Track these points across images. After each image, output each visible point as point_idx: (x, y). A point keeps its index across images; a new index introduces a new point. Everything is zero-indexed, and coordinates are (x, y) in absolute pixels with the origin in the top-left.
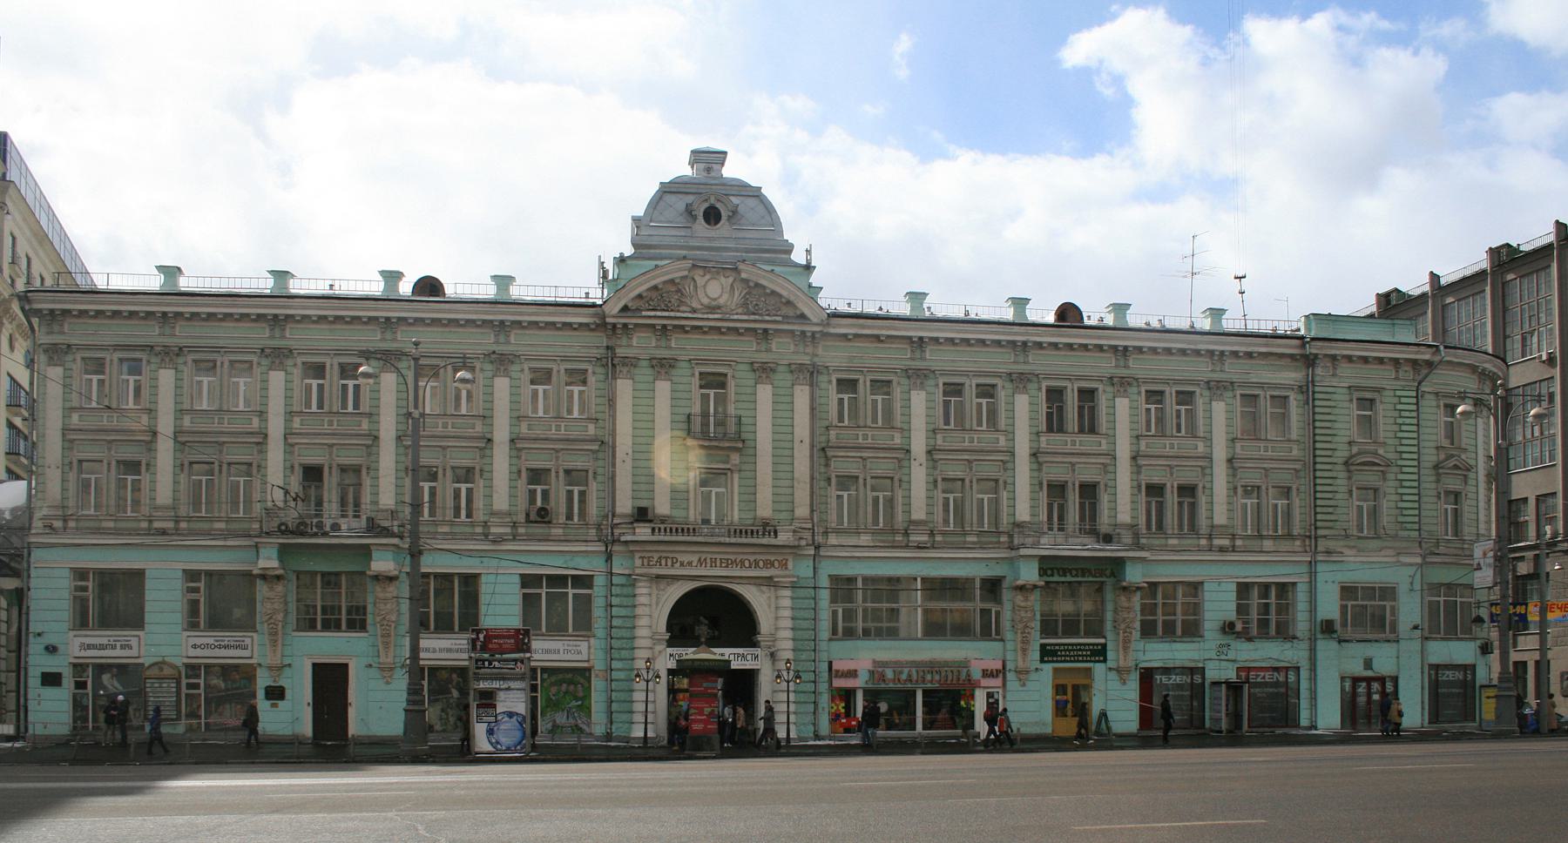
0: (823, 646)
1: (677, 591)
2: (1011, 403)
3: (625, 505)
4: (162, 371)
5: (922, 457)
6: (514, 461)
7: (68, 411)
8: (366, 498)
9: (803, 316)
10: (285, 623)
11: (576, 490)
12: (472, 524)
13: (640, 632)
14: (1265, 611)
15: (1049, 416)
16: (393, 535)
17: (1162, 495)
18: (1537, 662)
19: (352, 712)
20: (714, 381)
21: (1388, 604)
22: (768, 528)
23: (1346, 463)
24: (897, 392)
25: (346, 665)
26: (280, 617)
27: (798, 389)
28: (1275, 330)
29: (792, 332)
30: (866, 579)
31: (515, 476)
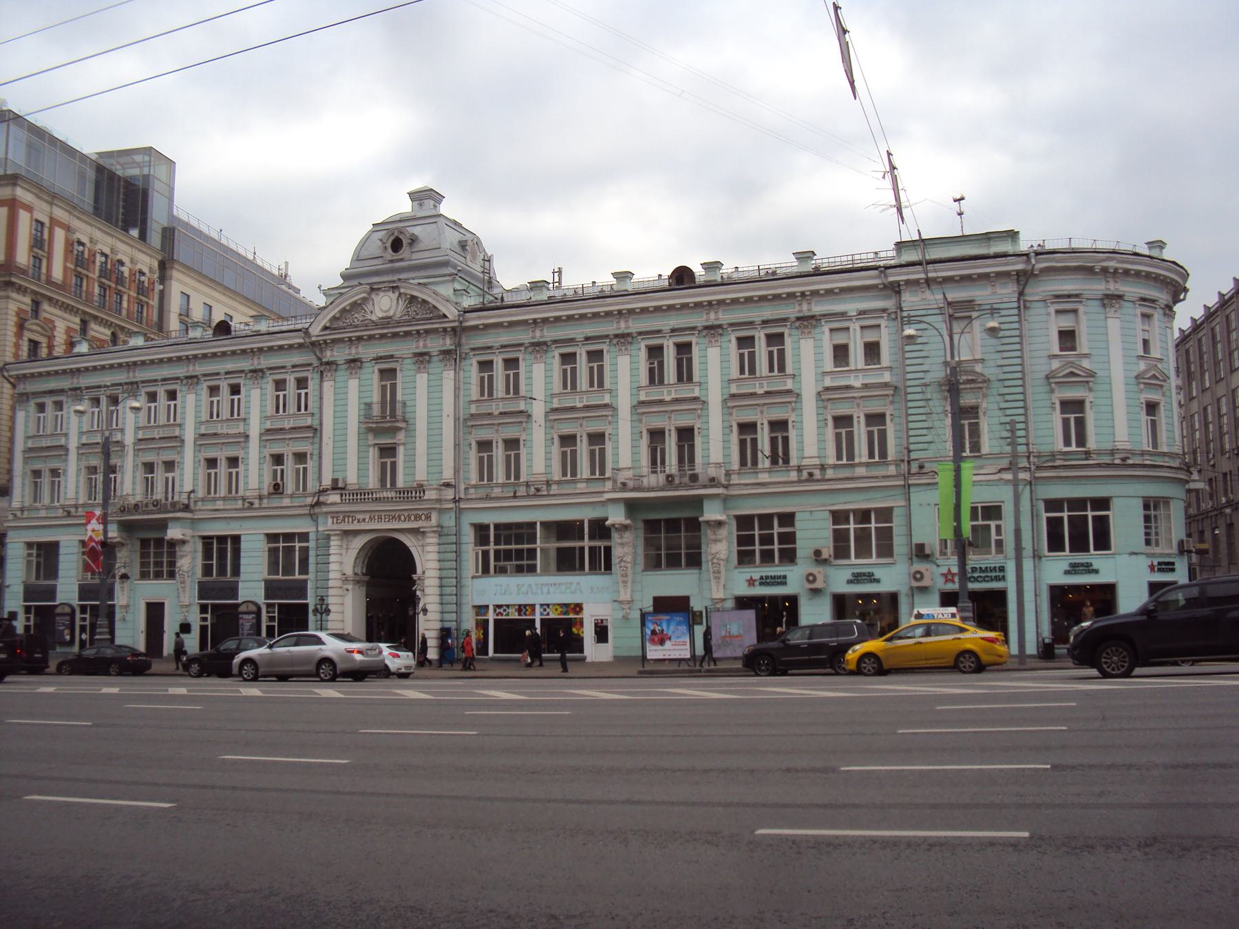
0: (467, 582)
1: (359, 542)
5: (541, 421)
7: (81, 433)
9: (445, 316)
10: (634, 563)
12: (886, 464)
13: (332, 575)
15: (651, 371)
18: (1174, 583)
20: (388, 374)
21: (993, 524)
22: (421, 488)
23: (1047, 377)
25: (163, 604)
26: (629, 559)
27: (445, 374)
30: (497, 526)
31: (549, 443)
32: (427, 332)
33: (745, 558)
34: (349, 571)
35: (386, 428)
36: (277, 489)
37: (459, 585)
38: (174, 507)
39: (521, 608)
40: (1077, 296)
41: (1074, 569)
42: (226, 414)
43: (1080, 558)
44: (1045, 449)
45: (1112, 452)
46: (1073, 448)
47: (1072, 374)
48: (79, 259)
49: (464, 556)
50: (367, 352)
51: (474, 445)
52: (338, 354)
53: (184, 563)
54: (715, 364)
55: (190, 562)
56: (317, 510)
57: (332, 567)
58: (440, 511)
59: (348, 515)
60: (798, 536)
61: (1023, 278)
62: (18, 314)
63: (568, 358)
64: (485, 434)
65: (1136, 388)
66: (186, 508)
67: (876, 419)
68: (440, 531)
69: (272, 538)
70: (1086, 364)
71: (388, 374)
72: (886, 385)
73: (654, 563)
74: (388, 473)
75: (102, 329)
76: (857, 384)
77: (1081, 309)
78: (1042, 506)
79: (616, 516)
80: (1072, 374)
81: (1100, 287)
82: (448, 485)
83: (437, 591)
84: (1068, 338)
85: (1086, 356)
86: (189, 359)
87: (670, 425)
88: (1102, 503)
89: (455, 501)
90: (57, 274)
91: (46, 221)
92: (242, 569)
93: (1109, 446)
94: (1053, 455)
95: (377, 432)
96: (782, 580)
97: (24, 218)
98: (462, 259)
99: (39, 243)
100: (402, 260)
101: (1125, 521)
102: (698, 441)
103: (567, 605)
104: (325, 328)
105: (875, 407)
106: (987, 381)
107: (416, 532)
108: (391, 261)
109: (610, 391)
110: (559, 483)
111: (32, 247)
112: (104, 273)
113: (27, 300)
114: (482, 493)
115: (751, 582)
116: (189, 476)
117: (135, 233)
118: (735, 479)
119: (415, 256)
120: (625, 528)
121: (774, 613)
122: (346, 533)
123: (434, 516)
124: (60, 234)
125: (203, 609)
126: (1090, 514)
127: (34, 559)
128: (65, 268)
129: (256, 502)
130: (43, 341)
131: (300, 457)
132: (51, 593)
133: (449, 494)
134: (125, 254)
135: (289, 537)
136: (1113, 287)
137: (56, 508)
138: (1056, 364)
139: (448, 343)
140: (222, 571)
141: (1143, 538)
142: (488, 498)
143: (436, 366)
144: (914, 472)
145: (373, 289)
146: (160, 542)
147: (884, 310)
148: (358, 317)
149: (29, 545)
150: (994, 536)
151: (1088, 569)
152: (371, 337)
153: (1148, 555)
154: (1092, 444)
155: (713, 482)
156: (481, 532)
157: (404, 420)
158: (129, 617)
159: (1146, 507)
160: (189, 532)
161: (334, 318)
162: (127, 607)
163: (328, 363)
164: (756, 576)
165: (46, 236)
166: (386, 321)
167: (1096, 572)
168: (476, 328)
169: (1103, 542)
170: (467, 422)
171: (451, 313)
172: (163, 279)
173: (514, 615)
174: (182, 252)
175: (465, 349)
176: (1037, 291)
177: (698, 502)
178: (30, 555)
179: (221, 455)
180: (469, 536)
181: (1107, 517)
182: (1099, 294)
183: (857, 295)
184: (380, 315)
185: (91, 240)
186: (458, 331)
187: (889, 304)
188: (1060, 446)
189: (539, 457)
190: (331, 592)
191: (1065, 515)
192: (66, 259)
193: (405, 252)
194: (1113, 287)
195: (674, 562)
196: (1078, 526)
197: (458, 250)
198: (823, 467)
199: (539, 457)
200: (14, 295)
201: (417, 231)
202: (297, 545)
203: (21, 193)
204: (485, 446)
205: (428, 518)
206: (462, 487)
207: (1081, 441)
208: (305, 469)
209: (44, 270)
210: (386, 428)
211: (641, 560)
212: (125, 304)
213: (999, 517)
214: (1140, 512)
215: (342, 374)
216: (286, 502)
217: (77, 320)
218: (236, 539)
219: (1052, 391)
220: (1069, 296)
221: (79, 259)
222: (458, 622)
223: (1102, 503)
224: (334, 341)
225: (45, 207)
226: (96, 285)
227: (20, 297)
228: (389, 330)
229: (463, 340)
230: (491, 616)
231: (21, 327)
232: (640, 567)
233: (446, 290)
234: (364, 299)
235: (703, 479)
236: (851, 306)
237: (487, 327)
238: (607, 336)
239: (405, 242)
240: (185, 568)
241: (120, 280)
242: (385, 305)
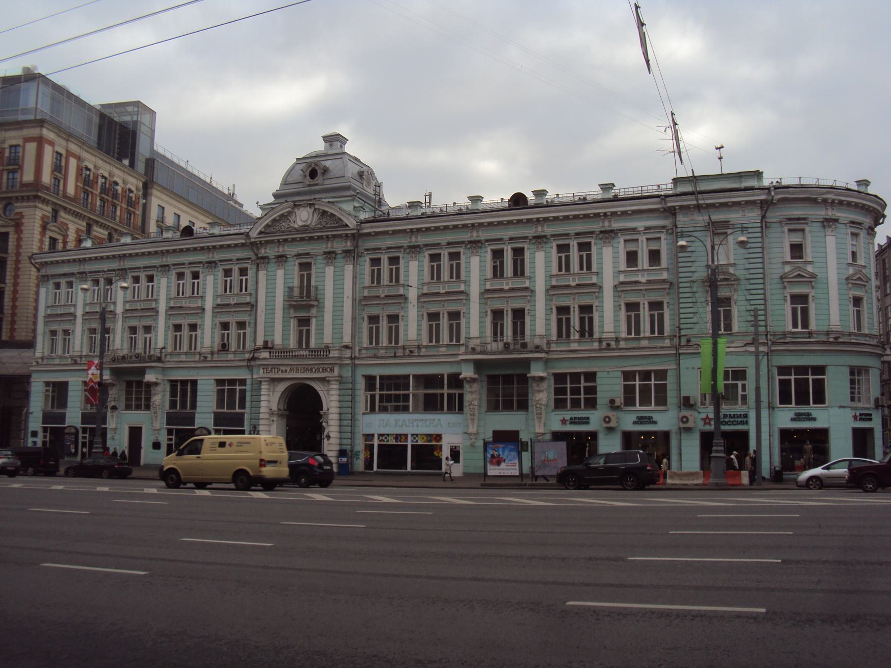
0: (359, 417)
1: (282, 387)
2: (600, 255)
3: (260, 343)
4: (327, 268)
6: (617, 299)
8: (596, 329)
9: (347, 226)
11: (586, 316)
14: (645, 387)
15: (495, 268)
16: (542, 351)
17: (569, 313)
19: (142, 451)
20: (305, 267)
21: (740, 383)
22: (327, 349)
23: (781, 278)
24: (594, 249)
25: (141, 428)
26: (476, 403)
28: (460, 210)
29: (341, 235)
30: (382, 377)
31: (420, 318)
32: (334, 236)
33: (559, 404)
34: (275, 407)
35: (303, 304)
36: (224, 347)
37: (353, 419)
38: (151, 358)
39: (397, 437)
40: (804, 219)
41: (798, 417)
42: (188, 293)
43: (803, 409)
44: (779, 329)
45: (828, 333)
46: (799, 329)
47: (799, 276)
48: (86, 180)
49: (357, 399)
50: (290, 250)
51: (366, 319)
52: (270, 252)
53: (157, 399)
54: (541, 264)
55: (161, 398)
56: (252, 363)
57: (263, 404)
58: (341, 366)
59: (274, 367)
60: (598, 389)
61: (765, 206)
62: (42, 219)
63: (435, 258)
64: (374, 311)
65: (846, 287)
66: (159, 360)
67: (656, 306)
68: (341, 380)
69: (220, 382)
70: (810, 268)
71: (305, 267)
72: (664, 281)
73: (494, 406)
74: (303, 338)
75: (101, 231)
76: (643, 280)
77: (807, 229)
78: (775, 371)
79: (467, 372)
80: (799, 276)
81: (821, 213)
82: (346, 347)
83: (337, 423)
84: (797, 250)
85: (810, 263)
86: (163, 253)
87: (508, 307)
88: (820, 370)
89: (352, 358)
90: (71, 190)
91: (63, 152)
92: (198, 404)
93: (825, 328)
94: (784, 334)
95: (296, 308)
96: (585, 421)
97: (48, 150)
98: (360, 185)
99: (59, 168)
100: (317, 185)
101: (836, 384)
102: (528, 319)
103: (430, 435)
104: (261, 233)
105: (655, 297)
106: (738, 279)
107: (323, 380)
108: (309, 185)
109: (465, 282)
110: (426, 347)
111: (53, 172)
112: (104, 190)
113: (49, 209)
114: (371, 353)
115: (564, 422)
116: (161, 337)
117: (126, 162)
118: (554, 347)
119: (326, 182)
120: (473, 380)
121: (580, 444)
122: (273, 381)
123: (336, 370)
124: (73, 162)
125: (170, 432)
126: (811, 377)
127: (50, 394)
128: (76, 186)
129: (209, 356)
130: (60, 238)
131: (241, 325)
132: (62, 418)
133: (348, 353)
134: (119, 177)
135: (232, 382)
136: (831, 213)
137: (67, 358)
138: (788, 268)
139: (349, 245)
140: (184, 405)
141: (849, 396)
142: (375, 357)
143: (340, 261)
144: (683, 345)
145: (296, 205)
146: (140, 383)
147: (664, 227)
148: (284, 225)
149: (47, 384)
150: (740, 392)
151: (809, 417)
152: (294, 240)
153: (853, 408)
154: (813, 326)
155: (538, 349)
156: (370, 381)
157: (316, 300)
158: (117, 437)
159: (852, 373)
160: (160, 377)
161: (267, 226)
162: (115, 429)
163: (263, 258)
164: (568, 417)
165: (63, 164)
166: (305, 229)
167: (815, 419)
168: (369, 234)
169: (820, 398)
170: (360, 302)
171: (352, 223)
172: (146, 195)
173: (392, 442)
174: (159, 176)
175: (361, 249)
176: (773, 215)
177: (526, 363)
178: (47, 391)
179: (185, 322)
180: (361, 384)
181: (823, 379)
182: (821, 218)
183: (644, 216)
184: (301, 224)
185: (95, 167)
186: (357, 236)
187: (667, 222)
188: (790, 328)
189: (413, 328)
190: (261, 422)
191: (793, 377)
192: (77, 180)
193: (319, 179)
194: (831, 213)
195: (508, 406)
196: (802, 385)
197: (358, 178)
198: (617, 340)
199: (413, 328)
200: (40, 205)
201: (328, 164)
202: (238, 388)
203: (47, 133)
204: (374, 319)
205: (332, 370)
206: (357, 349)
207: (805, 325)
208: (244, 333)
209: (61, 188)
210: (303, 304)
211: (484, 404)
212: (118, 213)
213: (744, 378)
214: (848, 377)
215: (272, 266)
216: (231, 357)
217: (84, 224)
218: (194, 383)
219: (785, 288)
220: (799, 219)
221: (86, 180)
222: (352, 445)
223: (820, 370)
224: (267, 242)
225: (63, 142)
226: (98, 198)
227: (44, 207)
228: (306, 235)
229: (360, 243)
230: (376, 442)
231: (44, 228)
232: (484, 409)
233: (348, 207)
234: (290, 213)
235: (530, 346)
236: (640, 224)
237: (377, 234)
238: (463, 242)
239: (319, 172)
240: (157, 403)
241: (115, 195)
242: (304, 217)
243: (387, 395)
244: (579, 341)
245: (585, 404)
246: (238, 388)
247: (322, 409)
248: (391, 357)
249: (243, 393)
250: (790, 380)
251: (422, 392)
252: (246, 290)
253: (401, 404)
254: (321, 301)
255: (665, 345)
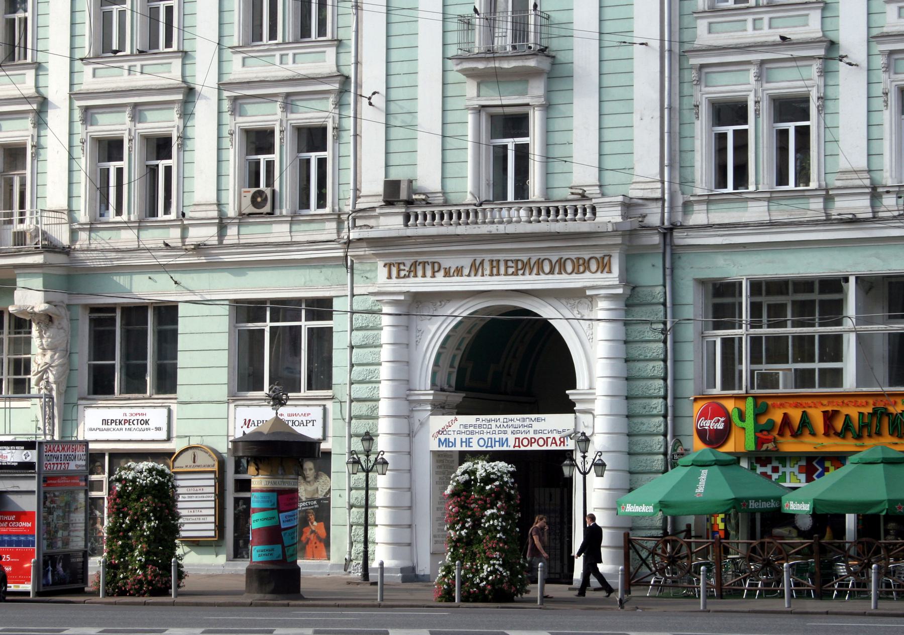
51: (705, 111)
69: (246, 310)
180: (693, 304)
191: (267, 325)
218: (168, 313)
243: (770, 339)
244: (771, 198)
245: (803, 371)
246: (305, 325)
247: (574, 387)
248: (816, 223)
249: (322, 340)
250: (311, 330)
251: (885, 328)
252: (168, 44)
253: (817, 365)
254: (561, 57)
255: (809, 216)
